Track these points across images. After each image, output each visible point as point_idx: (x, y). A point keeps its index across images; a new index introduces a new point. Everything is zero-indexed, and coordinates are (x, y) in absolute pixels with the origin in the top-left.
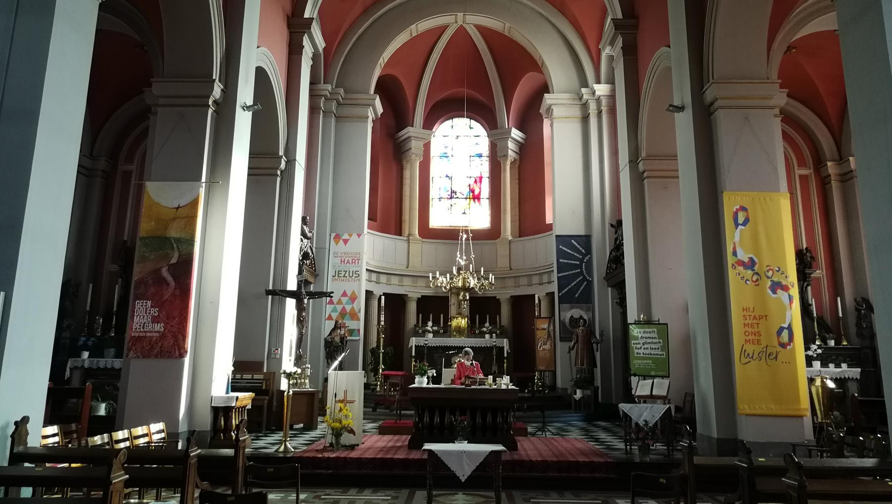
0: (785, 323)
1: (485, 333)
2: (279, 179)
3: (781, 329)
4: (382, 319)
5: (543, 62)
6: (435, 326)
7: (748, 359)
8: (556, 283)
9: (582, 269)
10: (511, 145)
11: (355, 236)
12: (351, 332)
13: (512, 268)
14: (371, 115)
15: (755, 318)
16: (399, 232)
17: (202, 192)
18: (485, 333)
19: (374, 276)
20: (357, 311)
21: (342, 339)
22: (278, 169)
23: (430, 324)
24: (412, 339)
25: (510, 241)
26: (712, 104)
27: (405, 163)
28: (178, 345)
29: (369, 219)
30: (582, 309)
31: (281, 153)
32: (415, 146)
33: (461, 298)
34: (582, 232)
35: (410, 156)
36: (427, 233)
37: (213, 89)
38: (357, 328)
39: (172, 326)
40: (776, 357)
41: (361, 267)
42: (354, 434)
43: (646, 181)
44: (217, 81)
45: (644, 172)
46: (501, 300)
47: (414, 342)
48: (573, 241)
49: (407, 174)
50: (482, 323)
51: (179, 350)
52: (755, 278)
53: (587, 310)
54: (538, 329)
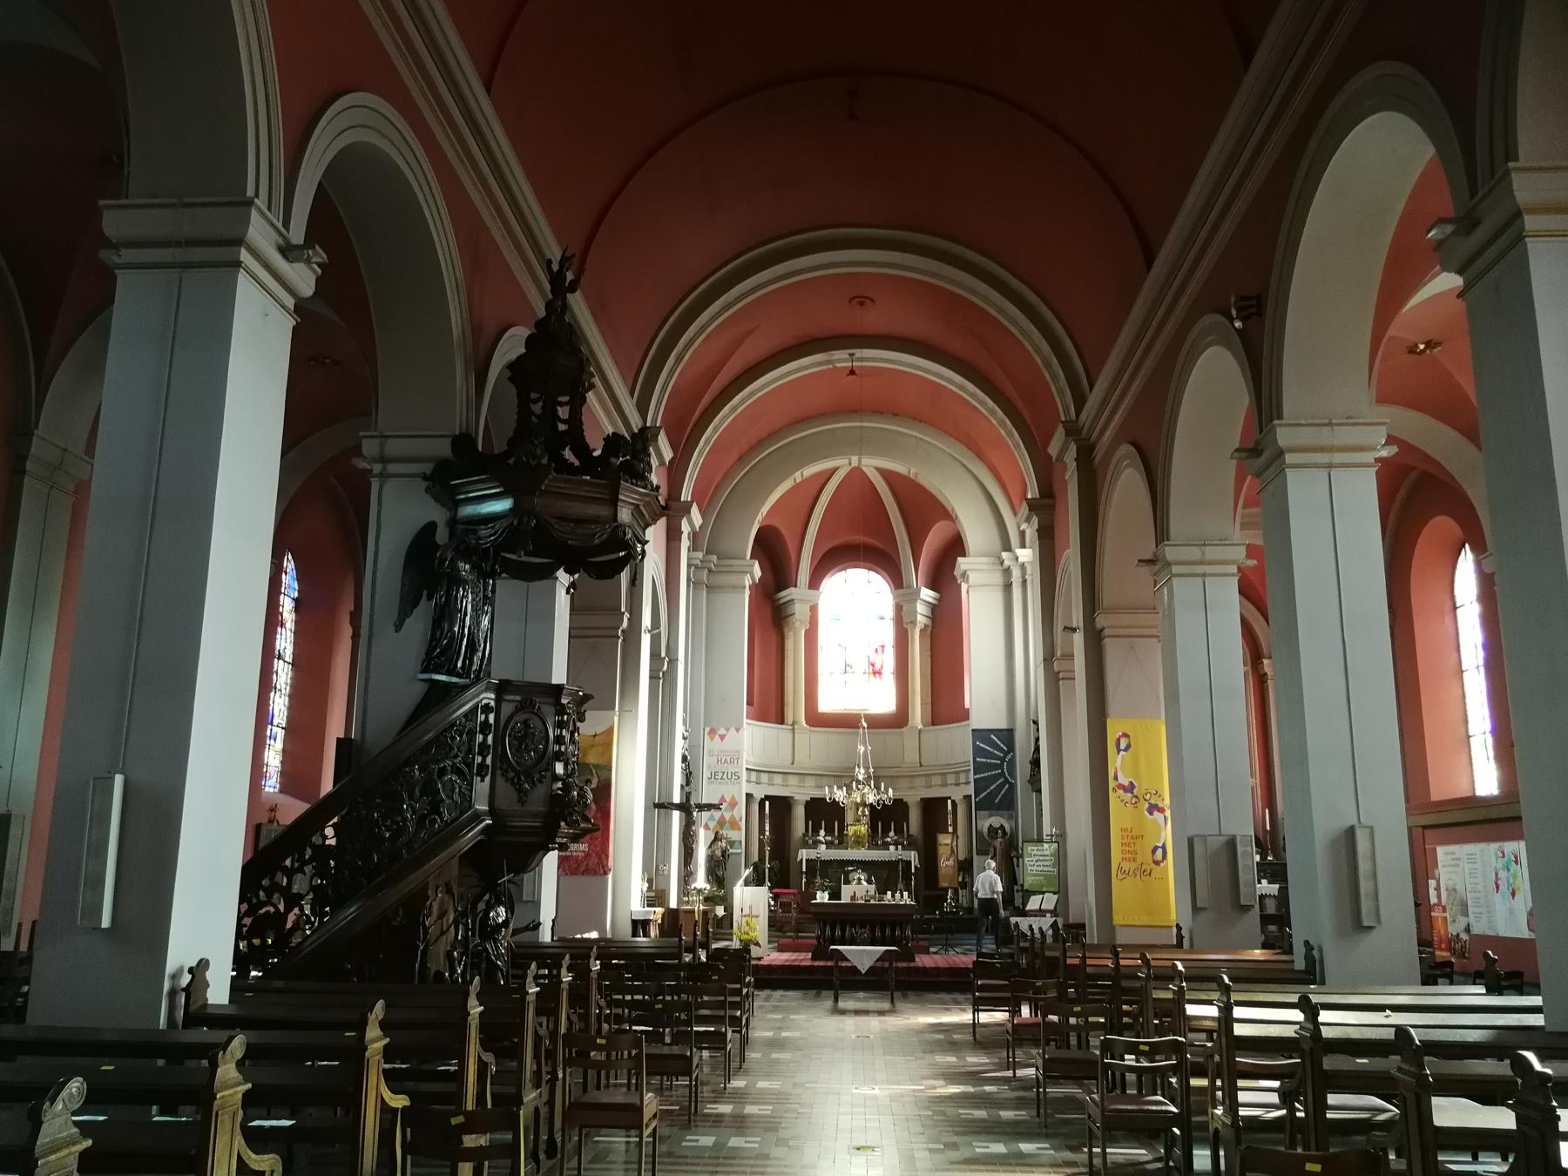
0: (1160, 842)
1: (889, 844)
2: (661, 681)
3: (1156, 848)
4: (767, 828)
5: (956, 517)
6: (829, 836)
7: (1124, 876)
8: (972, 784)
9: (1003, 770)
10: (921, 608)
11: (733, 730)
12: (732, 843)
13: (923, 764)
14: (748, 582)
15: (1132, 837)
16: (781, 720)
17: (616, 719)
18: (889, 844)
19: (754, 774)
20: (737, 819)
21: (724, 852)
22: (660, 670)
23: (822, 833)
24: (802, 852)
25: (920, 731)
26: (1102, 630)
27: (786, 630)
28: (602, 863)
29: (747, 704)
30: (1001, 816)
31: (663, 655)
32: (800, 611)
33: (860, 813)
34: (1003, 725)
35: (794, 623)
36: (817, 720)
37: (249, 222)
38: (738, 839)
39: (595, 846)
40: (1150, 874)
41: (741, 767)
42: (760, 947)
43: (1061, 682)
44: (261, 202)
45: (1059, 672)
46: (909, 804)
47: (804, 854)
48: (992, 736)
49: (789, 644)
50: (886, 832)
51: (603, 868)
52: (1133, 801)
53: (1010, 818)
54: (941, 845)
